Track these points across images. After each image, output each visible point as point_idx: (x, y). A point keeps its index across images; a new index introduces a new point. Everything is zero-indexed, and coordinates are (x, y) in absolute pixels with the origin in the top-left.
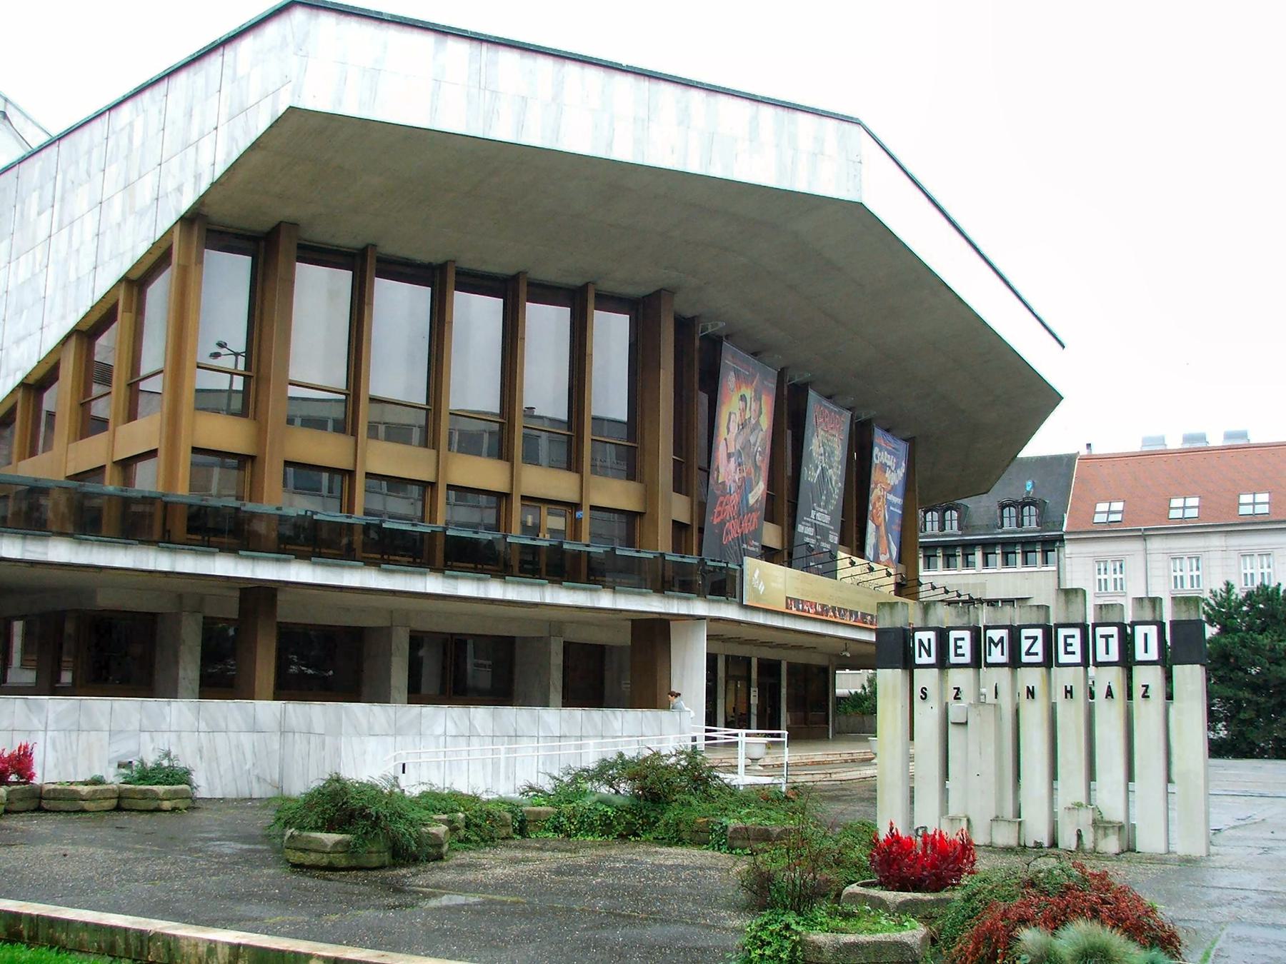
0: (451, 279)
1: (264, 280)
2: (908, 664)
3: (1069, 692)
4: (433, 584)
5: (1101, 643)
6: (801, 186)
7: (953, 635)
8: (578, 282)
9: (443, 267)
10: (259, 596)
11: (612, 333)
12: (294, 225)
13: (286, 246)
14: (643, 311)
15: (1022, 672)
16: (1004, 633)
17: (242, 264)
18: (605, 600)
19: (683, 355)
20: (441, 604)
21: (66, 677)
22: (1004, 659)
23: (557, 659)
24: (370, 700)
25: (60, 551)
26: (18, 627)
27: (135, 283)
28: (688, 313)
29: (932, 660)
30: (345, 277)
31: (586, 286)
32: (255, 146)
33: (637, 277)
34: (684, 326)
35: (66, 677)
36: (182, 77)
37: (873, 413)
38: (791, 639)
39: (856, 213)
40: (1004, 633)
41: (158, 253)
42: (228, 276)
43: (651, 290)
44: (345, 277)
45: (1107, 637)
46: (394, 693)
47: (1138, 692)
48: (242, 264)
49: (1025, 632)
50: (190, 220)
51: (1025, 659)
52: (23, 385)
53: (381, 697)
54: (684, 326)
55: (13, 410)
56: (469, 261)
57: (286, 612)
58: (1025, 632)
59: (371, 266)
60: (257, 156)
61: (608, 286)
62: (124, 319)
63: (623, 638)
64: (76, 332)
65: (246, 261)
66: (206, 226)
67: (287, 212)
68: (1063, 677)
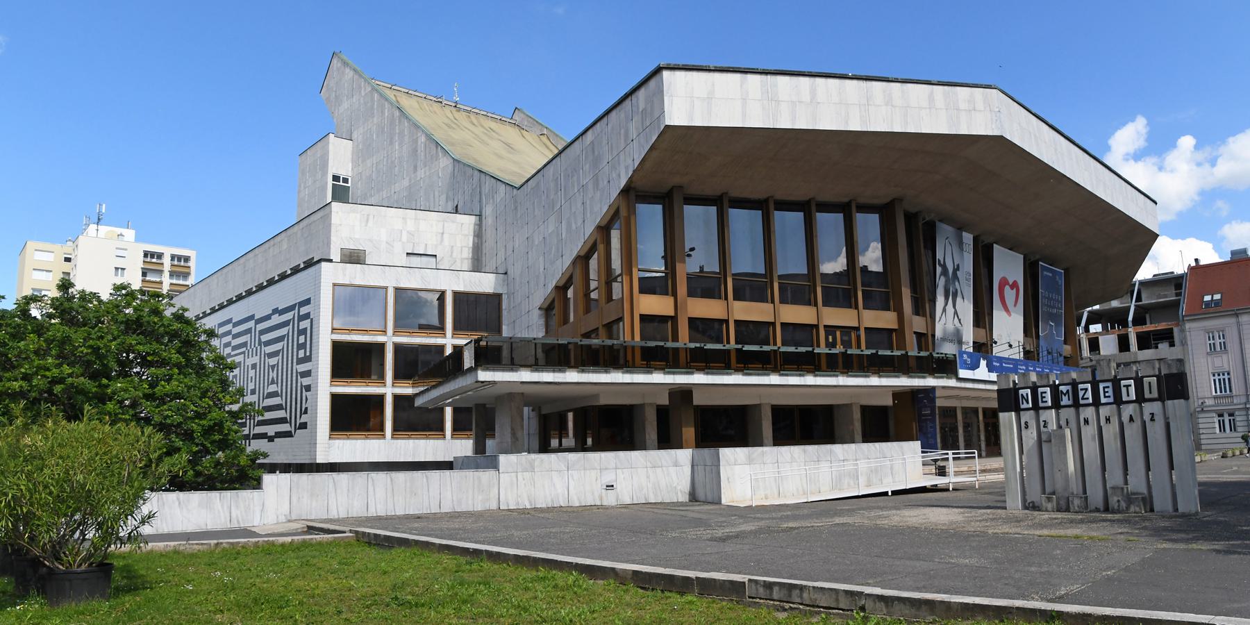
0: (772, 206)
1: (254, 534)
2: (1018, 410)
3: (1108, 420)
4: (774, 379)
5: (1124, 390)
6: (964, 131)
7: (1040, 390)
8: (846, 200)
9: (766, 201)
10: (683, 394)
11: (868, 224)
12: (681, 187)
13: (677, 198)
14: (886, 212)
15: (1062, 411)
16: (1069, 387)
17: (658, 208)
18: (874, 381)
19: (913, 233)
20: (781, 389)
21: (589, 441)
22: (1070, 403)
23: (857, 415)
24: (843, 442)
25: (572, 376)
26: (570, 416)
27: (604, 230)
28: (913, 210)
29: (1030, 405)
30: (713, 210)
31: (850, 202)
32: (652, 148)
33: (883, 194)
34: (911, 218)
35: (589, 441)
36: (614, 114)
37: (1037, 257)
38: (973, 394)
39: (1000, 143)
40: (1069, 387)
41: (612, 212)
42: (650, 217)
43: (887, 200)
44: (713, 210)
45: (1127, 386)
46: (765, 441)
47: (1023, 425)
48: (658, 208)
49: (1081, 386)
50: (626, 191)
51: (1082, 402)
52: (557, 287)
53: (643, 447)
54: (911, 218)
55: (553, 301)
56: (781, 195)
57: (698, 400)
58: (1081, 386)
59: (726, 203)
60: (655, 154)
61: (862, 200)
62: (601, 247)
63: (889, 402)
64: (578, 257)
65: (659, 208)
66: (633, 193)
67: (676, 180)
68: (1128, 410)
